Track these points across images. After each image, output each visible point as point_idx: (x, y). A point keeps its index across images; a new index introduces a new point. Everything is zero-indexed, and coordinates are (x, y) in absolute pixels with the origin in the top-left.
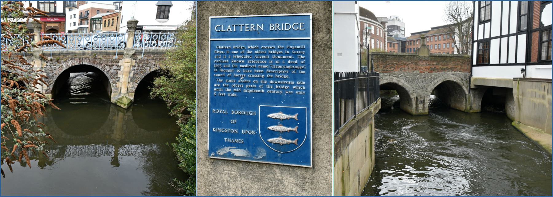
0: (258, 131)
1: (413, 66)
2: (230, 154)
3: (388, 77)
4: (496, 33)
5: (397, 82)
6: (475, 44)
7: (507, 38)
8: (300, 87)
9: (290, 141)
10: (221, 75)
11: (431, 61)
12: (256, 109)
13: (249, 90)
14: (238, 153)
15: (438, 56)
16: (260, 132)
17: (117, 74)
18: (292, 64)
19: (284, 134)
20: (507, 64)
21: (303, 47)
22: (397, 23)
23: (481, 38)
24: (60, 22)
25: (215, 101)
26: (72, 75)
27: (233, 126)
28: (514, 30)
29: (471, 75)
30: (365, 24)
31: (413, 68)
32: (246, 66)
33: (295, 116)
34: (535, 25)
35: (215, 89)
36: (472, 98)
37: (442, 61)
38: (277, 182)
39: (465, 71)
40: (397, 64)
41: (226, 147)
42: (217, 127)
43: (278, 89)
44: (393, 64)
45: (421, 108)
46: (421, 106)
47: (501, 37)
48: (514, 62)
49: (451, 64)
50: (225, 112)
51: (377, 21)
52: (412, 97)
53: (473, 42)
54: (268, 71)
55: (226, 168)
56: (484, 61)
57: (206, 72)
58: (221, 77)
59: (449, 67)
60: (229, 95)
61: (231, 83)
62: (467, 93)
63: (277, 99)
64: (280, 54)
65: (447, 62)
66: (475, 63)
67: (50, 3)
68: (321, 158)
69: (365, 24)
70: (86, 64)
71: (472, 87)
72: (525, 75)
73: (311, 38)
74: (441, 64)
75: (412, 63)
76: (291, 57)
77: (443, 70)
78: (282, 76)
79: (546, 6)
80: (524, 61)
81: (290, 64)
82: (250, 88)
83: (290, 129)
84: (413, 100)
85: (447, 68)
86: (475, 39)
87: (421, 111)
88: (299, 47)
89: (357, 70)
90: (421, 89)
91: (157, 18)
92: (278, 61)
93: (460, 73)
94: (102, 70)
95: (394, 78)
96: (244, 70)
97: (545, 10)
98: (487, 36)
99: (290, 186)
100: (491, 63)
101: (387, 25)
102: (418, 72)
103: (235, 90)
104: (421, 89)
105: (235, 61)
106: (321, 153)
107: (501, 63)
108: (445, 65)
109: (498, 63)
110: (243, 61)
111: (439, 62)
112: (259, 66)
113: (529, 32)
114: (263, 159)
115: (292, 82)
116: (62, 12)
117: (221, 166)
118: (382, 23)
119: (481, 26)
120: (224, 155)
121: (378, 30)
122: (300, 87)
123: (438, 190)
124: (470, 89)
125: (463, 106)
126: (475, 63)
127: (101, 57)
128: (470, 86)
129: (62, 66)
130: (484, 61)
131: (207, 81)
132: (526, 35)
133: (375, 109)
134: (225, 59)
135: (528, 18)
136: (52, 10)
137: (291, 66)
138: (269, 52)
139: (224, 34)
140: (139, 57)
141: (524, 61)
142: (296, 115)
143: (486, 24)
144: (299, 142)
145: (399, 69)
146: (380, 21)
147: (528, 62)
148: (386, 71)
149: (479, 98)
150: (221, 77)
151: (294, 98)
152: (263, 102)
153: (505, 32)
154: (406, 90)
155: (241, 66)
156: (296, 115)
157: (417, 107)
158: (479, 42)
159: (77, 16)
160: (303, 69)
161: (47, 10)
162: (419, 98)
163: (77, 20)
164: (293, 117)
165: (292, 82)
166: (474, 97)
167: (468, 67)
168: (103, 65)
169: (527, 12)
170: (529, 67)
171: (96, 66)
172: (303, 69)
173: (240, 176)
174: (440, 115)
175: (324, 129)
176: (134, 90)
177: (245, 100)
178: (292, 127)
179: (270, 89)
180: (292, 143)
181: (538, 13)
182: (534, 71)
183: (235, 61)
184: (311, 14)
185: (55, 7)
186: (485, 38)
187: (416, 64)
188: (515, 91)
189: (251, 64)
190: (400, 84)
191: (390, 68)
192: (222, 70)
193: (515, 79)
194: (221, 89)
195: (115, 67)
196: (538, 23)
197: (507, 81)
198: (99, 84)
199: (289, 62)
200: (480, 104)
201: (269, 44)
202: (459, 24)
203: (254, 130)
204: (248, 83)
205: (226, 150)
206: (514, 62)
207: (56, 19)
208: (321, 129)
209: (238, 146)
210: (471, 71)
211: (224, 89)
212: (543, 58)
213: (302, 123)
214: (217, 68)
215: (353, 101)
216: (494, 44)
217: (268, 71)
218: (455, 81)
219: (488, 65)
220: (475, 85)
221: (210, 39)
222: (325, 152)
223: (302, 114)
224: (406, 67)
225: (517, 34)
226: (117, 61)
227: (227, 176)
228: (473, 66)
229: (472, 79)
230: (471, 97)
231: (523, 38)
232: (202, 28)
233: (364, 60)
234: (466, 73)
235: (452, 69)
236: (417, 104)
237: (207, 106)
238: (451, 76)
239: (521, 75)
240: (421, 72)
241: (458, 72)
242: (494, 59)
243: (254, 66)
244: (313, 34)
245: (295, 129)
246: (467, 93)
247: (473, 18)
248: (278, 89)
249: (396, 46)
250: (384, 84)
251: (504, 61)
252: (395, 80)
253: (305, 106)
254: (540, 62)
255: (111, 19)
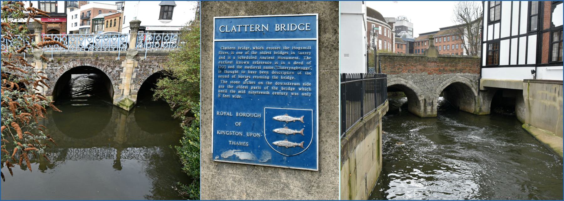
0: (263, 134)
1: (421, 67)
2: (234, 157)
3: (396, 79)
4: (505, 33)
5: (405, 84)
6: (485, 45)
7: (517, 39)
8: (306, 89)
9: (296, 144)
10: (226, 76)
11: (440, 62)
12: (261, 111)
13: (254, 92)
14: (243, 156)
15: (447, 58)
16: (265, 135)
17: (119, 76)
18: (298, 65)
19: (289, 137)
20: (517, 65)
21: (310, 48)
22: (405, 24)
23: (490, 38)
24: (61, 23)
25: (219, 103)
26: (73, 76)
27: (238, 129)
28: (524, 30)
29: (481, 76)
30: (373, 25)
31: (421, 70)
32: (251, 67)
33: (301, 119)
34: (546, 26)
35: (219, 91)
36: (482, 100)
37: (451, 62)
38: (282, 185)
39: (474, 72)
40: (405, 65)
41: (230, 150)
42: (222, 129)
43: (284, 91)
44: (400, 65)
45: (429, 111)
46: (429, 108)
47: (511, 37)
48: (524, 63)
49: (460, 66)
50: (229, 114)
51: (385, 21)
52: (420, 99)
53: (483, 43)
54: (273, 72)
55: (230, 171)
56: (493, 62)
57: (210, 74)
58: (225, 79)
59: (458, 68)
60: (233, 97)
61: (235, 85)
62: (476, 94)
63: (282, 101)
64: (286, 55)
65: (456, 63)
66: (484, 64)
67: (51, 3)
68: (328, 161)
69: (373, 25)
70: (88, 65)
71: (482, 88)
72: (535, 77)
73: (317, 39)
74: (450, 66)
75: (420, 64)
76: (297, 58)
77: (451, 71)
78: (288, 78)
79: (557, 6)
80: (534, 63)
81: (295, 65)
82: (255, 90)
83: (296, 131)
84: (421, 102)
85: (456, 69)
86: (485, 40)
87: (430, 113)
88: (305, 48)
89: (364, 71)
90: (430, 91)
91: (160, 19)
92: (284, 63)
93: (469, 74)
94: (105, 71)
95: (402, 79)
96: (249, 72)
97: (555, 10)
98: (497, 37)
99: (296, 190)
100: (501, 64)
101: (394, 25)
102: (427, 74)
103: (239, 92)
104: (430, 91)
105: (240, 62)
106: (328, 156)
107: (511, 64)
108: (453, 66)
109: (508, 64)
110: (248, 62)
111: (448, 63)
112: (264, 67)
113: (540, 33)
114: (268, 162)
115: (298, 84)
116: (63, 12)
117: (226, 170)
118: (389, 23)
119: (491, 27)
120: (229, 158)
121: (385, 31)
122: (306, 89)
123: (447, 194)
124: (480, 91)
125: (473, 108)
126: (484, 64)
127: (103, 58)
128: (479, 88)
129: (63, 68)
130: (493, 62)
131: (211, 83)
132: (536, 35)
133: (383, 111)
134: (229, 60)
135: (539, 18)
136: (53, 10)
137: (297, 68)
138: (275, 53)
139: (228, 35)
140: (142, 58)
141: (534, 62)
142: (302, 117)
143: (496, 25)
144: (305, 145)
145: (407, 71)
146: (387, 22)
147: (539, 63)
148: (394, 73)
149: (488, 100)
150: (225, 79)
151: (300, 100)
152: (268, 104)
153: (515, 33)
154: (414, 92)
155: (245, 67)
156: (302, 117)
157: (425, 109)
158: (488, 42)
159: (79, 17)
160: (309, 71)
161: (48, 11)
162: (427, 100)
163: (79, 21)
164: (299, 119)
165: (298, 84)
166: (484, 99)
167: (478, 69)
168: (105, 66)
169: (537, 13)
170: (539, 69)
171: (98, 67)
172: (309, 71)
173: (245, 179)
174: (448, 117)
175: (330, 131)
176: (137, 91)
177: (250, 102)
178: (298, 130)
179: (275, 91)
180: (298, 146)
181: (549, 13)
182: (545, 73)
183: (240, 62)
184: (317, 15)
185: (56, 7)
186: (495, 38)
187: (424, 65)
188: (525, 93)
189: (256, 65)
190: (408, 85)
191: (398, 69)
192: (226, 72)
193: (525, 81)
194: (226, 91)
195: (117, 69)
196: (549, 23)
197: (517, 83)
198: (101, 85)
199: (295, 63)
200: (490, 106)
201: (274, 45)
202: (468, 25)
203: (259, 132)
204: (253, 85)
205: (231, 153)
206: (524, 63)
207: (57, 20)
208: (328, 132)
209: (243, 149)
210: (480, 73)
211: (228, 91)
212: (554, 59)
213: (308, 126)
214: (221, 69)
215: (360, 103)
216: (504, 45)
217: (273, 72)
218: (464, 82)
219: (498, 66)
220: (485, 87)
221: (214, 40)
222: (332, 155)
223: (308, 116)
224: (415, 68)
225: (527, 35)
226: (120, 63)
227: (231, 179)
228: (482, 67)
229: (481, 81)
230: (480, 99)
231: (533, 39)
232: (206, 29)
233: (371, 62)
234: (475, 75)
235: (461, 71)
236: (425, 106)
237: (211, 108)
238: (460, 78)
239: (531, 77)
240: (429, 74)
241: (467, 74)
242: (503, 60)
243: (259, 67)
244: (319, 35)
245: (301, 132)
246: (476, 94)
247: (482, 18)
248: (284, 91)
249: (404, 47)
250: (392, 86)
251: (514, 62)
252: (403, 82)
253: (311, 108)
254: (551, 63)
255: (113, 19)
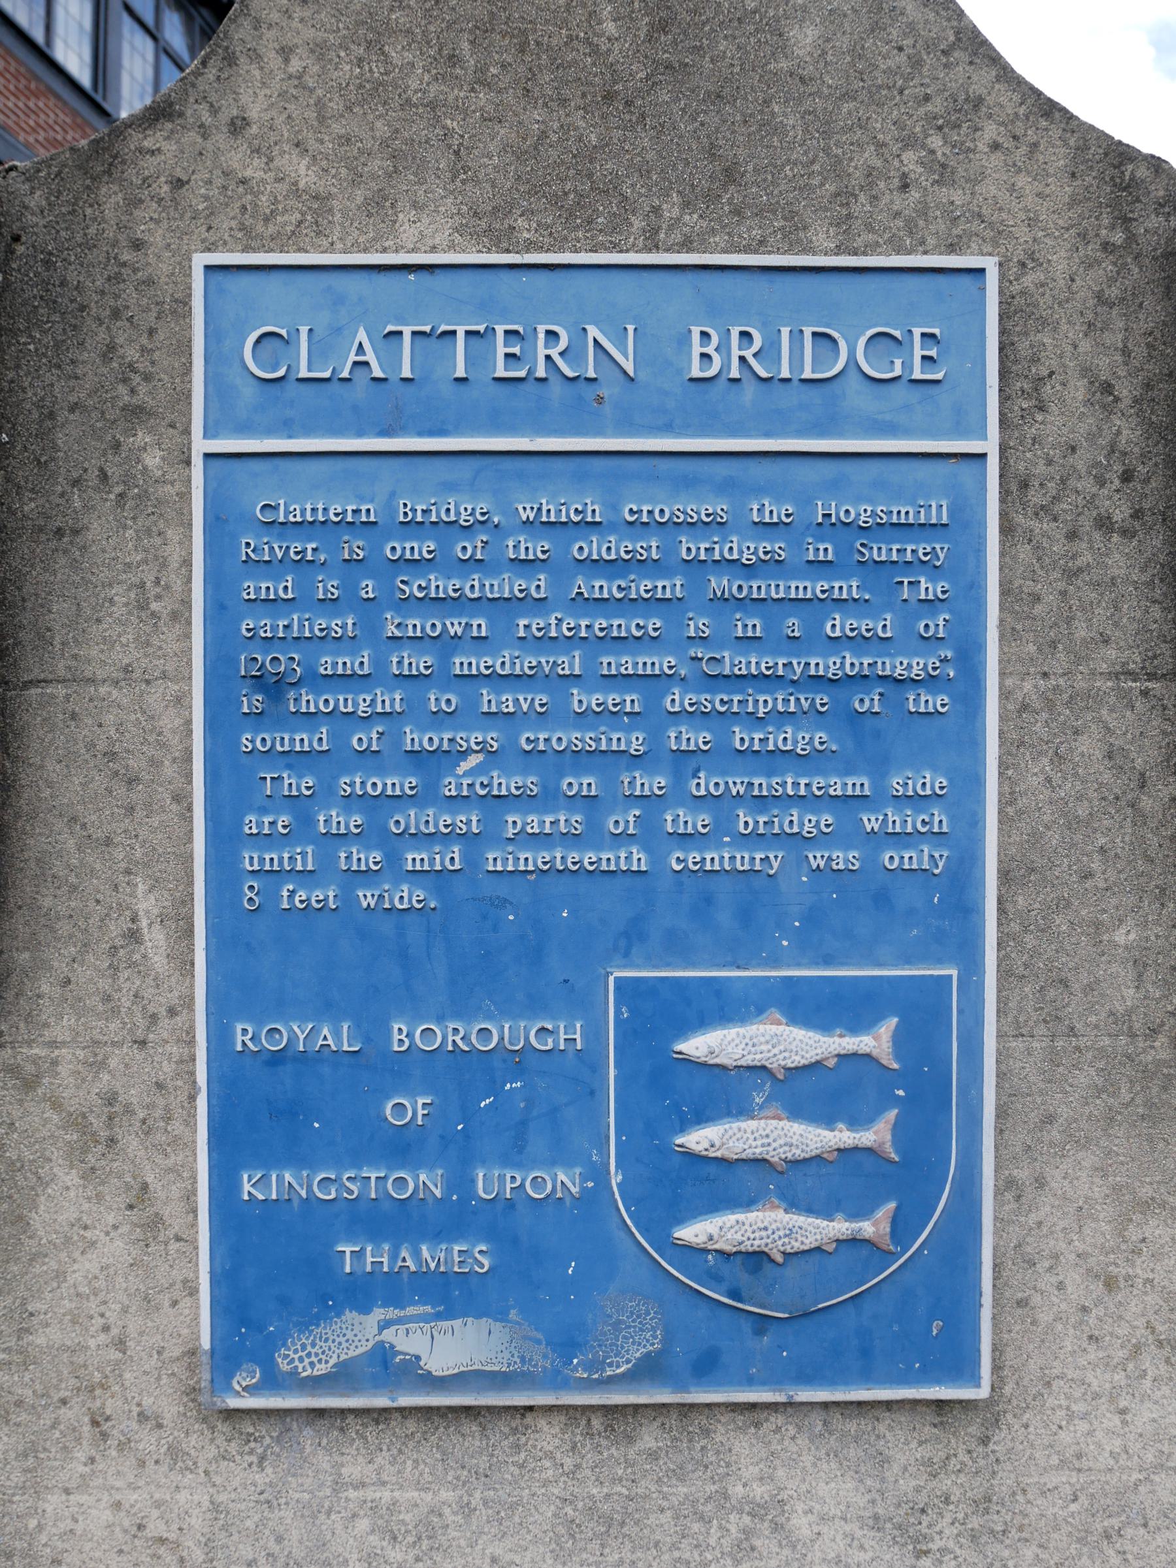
0: (599, 1174)
2: (386, 1366)
8: (913, 821)
9: (840, 1227)
10: (302, 740)
12: (580, 1000)
13: (532, 858)
14: (450, 1347)
16: (616, 1179)
18: (859, 642)
19: (789, 1181)
21: (938, 511)
25: (254, 950)
32: (504, 660)
33: (877, 1041)
35: (250, 859)
38: (736, 1523)
41: (350, 1316)
42: (280, 1162)
43: (753, 839)
50: (337, 1036)
54: (677, 699)
55: (353, 1470)
57: (169, 721)
58: (297, 759)
60: (366, 897)
61: (376, 805)
63: (741, 910)
64: (771, 566)
68: (1044, 1318)
73: (990, 445)
76: (850, 587)
81: (584, 718)
82: (540, 839)
83: (843, 1136)
88: (903, 511)
92: (755, 624)
96: (487, 699)
103: (414, 858)
105: (415, 624)
106: (1047, 1281)
110: (480, 625)
112: (610, 663)
114: (649, 1369)
115: (858, 783)
117: (323, 1460)
120: (343, 1376)
122: (913, 821)
131: (182, 798)
134: (330, 604)
137: (851, 662)
138: (688, 546)
139: (325, 399)
142: (888, 1027)
144: (902, 1229)
150: (297, 759)
151: (865, 904)
152: (630, 940)
155: (460, 663)
156: (888, 1027)
160: (930, 682)
164: (863, 1043)
165: (858, 783)
172: (930, 682)
173: (467, 1510)
175: (1064, 1112)
177: (491, 938)
178: (855, 1123)
179: (685, 839)
180: (854, 1241)
183: (415, 624)
184: (990, 264)
189: (544, 642)
192: (309, 701)
194: (306, 857)
199: (837, 624)
201: (687, 484)
203: (568, 1165)
204: (521, 800)
205: (357, 1333)
208: (1050, 1119)
209: (450, 1296)
211: (326, 861)
213: (925, 1087)
214: (258, 681)
217: (677, 699)
221: (200, 445)
223: (925, 1018)
227: (363, 1525)
232: (132, 353)
233: (209, 816)
237: (189, 1002)
243: (570, 662)
245: (877, 1134)
248: (753, 839)
